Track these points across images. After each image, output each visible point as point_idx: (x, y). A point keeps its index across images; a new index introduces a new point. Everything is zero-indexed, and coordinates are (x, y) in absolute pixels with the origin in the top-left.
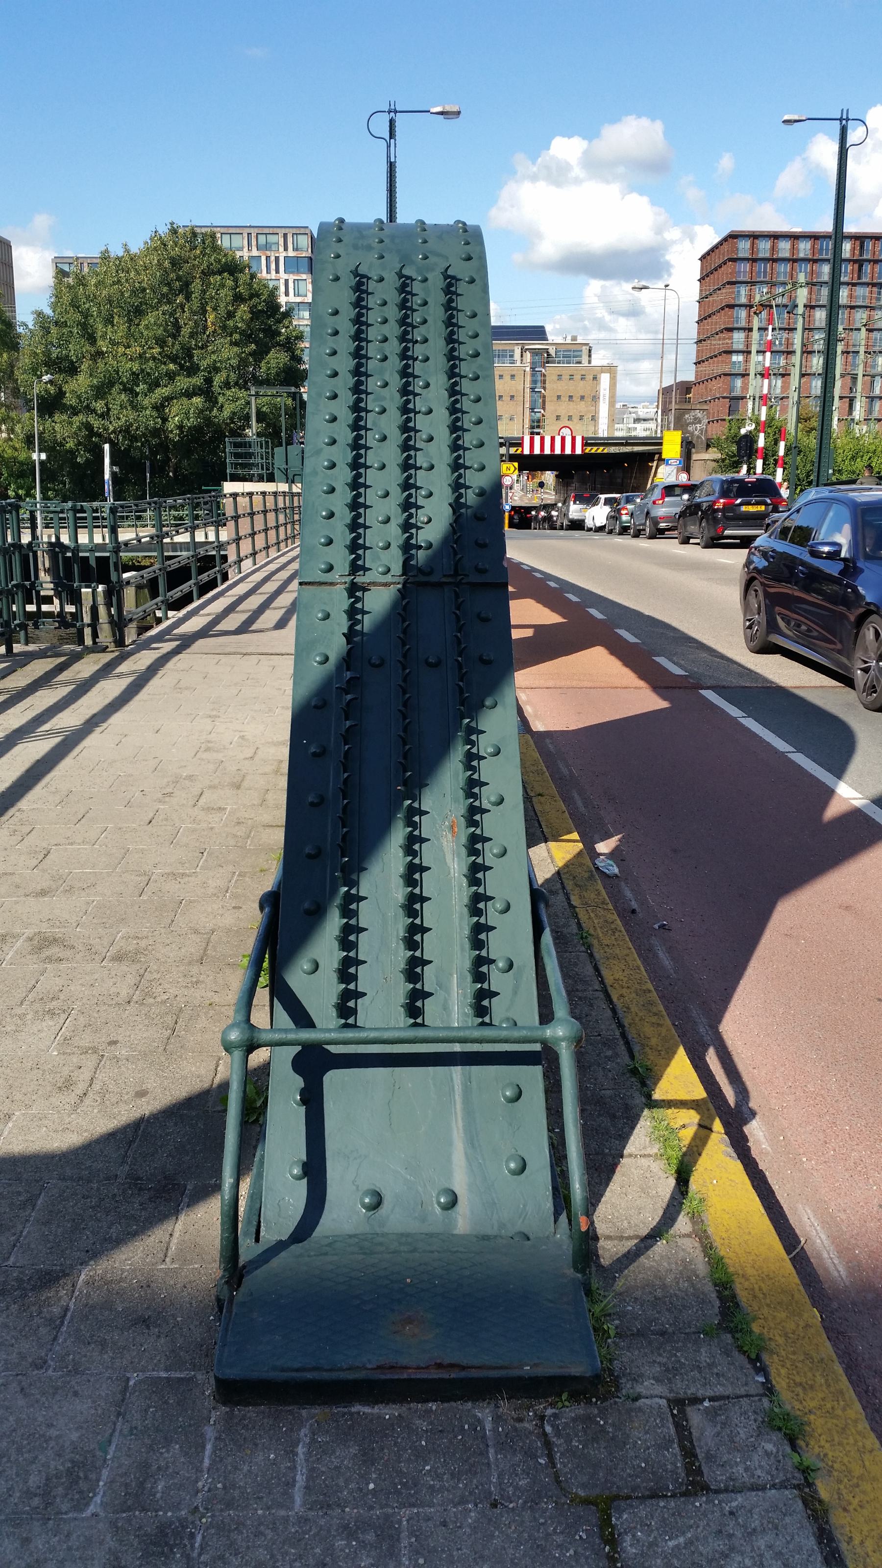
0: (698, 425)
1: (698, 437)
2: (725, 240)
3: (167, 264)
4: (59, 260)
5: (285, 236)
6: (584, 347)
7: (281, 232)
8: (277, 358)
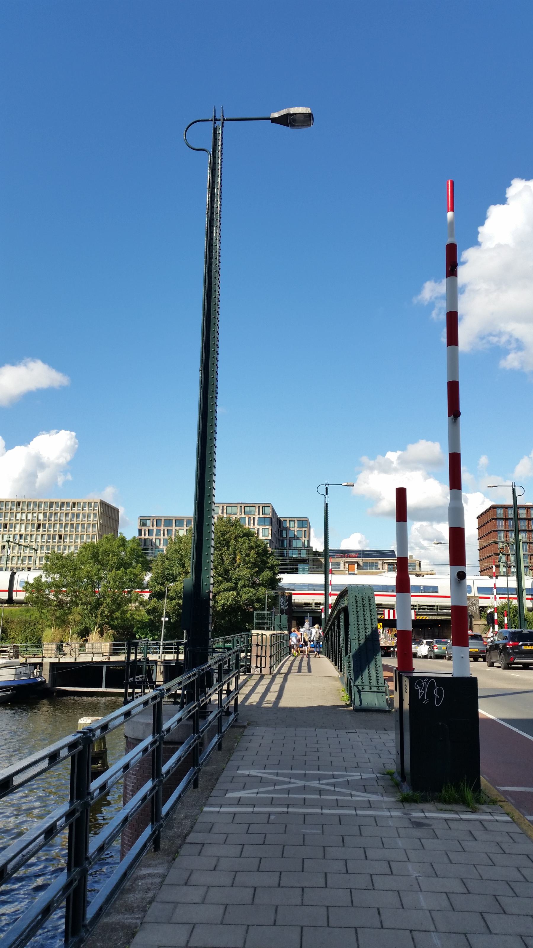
0: (474, 607)
1: (475, 613)
2: (489, 509)
3: (219, 534)
4: (142, 518)
5: (259, 508)
6: (417, 562)
7: (257, 506)
8: (267, 574)
